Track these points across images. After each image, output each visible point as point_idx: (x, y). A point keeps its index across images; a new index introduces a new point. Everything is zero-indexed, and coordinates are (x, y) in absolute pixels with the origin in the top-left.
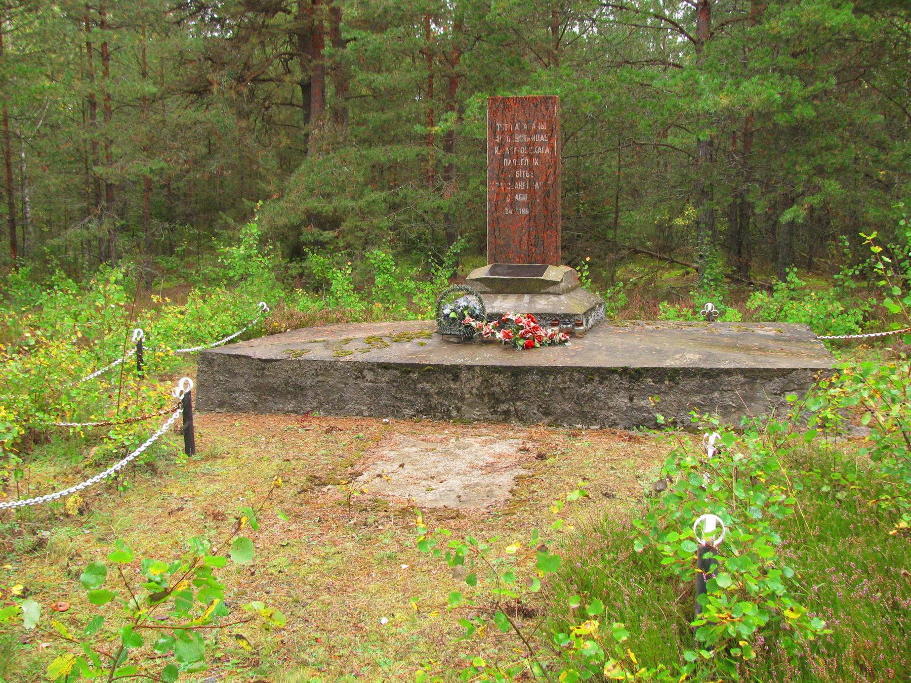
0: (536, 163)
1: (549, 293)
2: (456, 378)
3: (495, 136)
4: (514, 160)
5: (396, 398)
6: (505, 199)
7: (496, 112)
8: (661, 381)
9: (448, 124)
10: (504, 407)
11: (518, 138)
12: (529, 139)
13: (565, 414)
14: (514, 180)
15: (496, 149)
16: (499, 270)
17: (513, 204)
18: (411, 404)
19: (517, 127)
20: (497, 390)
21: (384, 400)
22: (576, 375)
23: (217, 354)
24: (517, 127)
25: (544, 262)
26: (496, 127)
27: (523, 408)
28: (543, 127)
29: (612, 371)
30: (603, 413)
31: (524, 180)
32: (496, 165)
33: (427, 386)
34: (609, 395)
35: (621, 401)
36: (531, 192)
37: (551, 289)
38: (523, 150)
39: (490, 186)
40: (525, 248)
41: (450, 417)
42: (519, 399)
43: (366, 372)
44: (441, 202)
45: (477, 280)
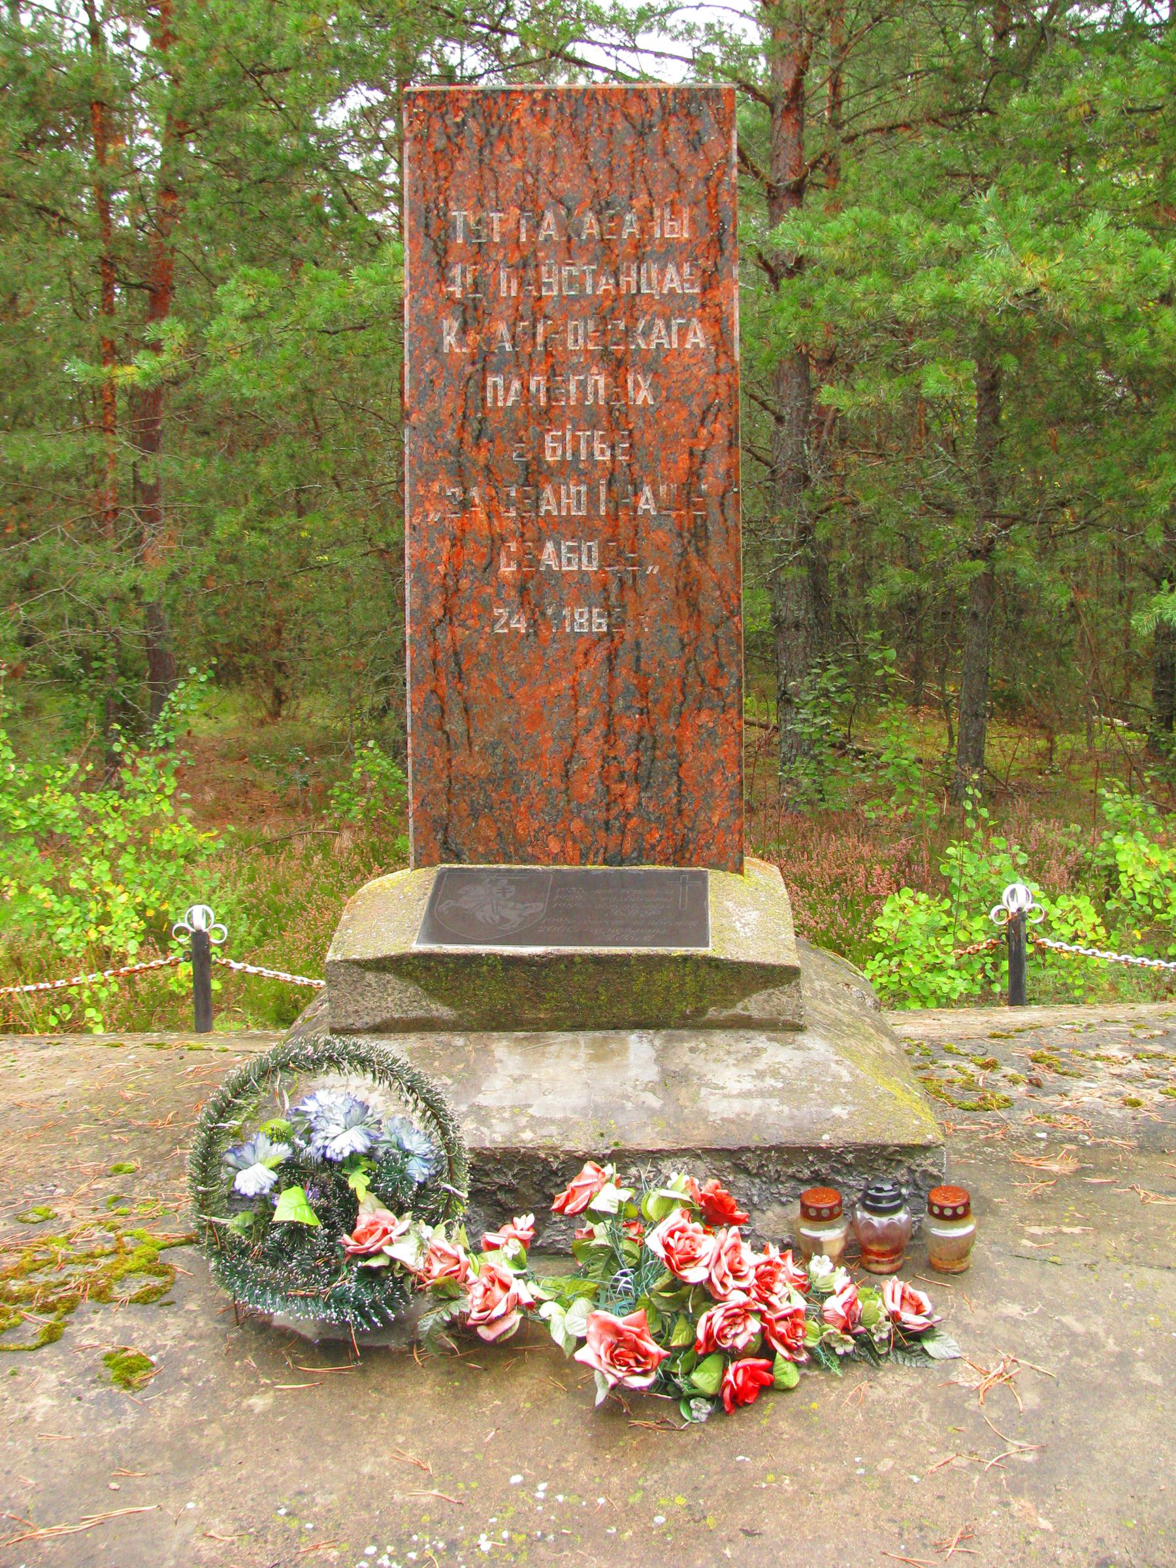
0: (643, 396)
3: (443, 268)
4: (537, 382)
6: (491, 564)
9: (165, 358)
11: (555, 280)
12: (605, 284)
14: (534, 474)
15: (450, 328)
16: (474, 899)
17: (531, 590)
19: (550, 227)
24: (550, 227)
25: (679, 855)
26: (448, 225)
31: (583, 476)
32: (447, 404)
36: (618, 534)
37: (754, 1005)
38: (578, 338)
39: (419, 502)
40: (589, 789)
44: (141, 578)
45: (380, 965)
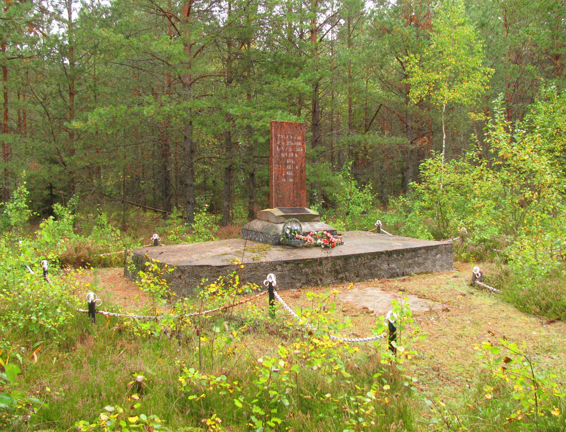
1: (315, 221)
2: (321, 264)
5: (293, 278)
7: (277, 128)
8: (398, 256)
10: (341, 276)
11: (288, 143)
13: (365, 275)
14: (286, 164)
15: (278, 147)
17: (286, 177)
18: (300, 280)
20: (338, 267)
21: (287, 280)
22: (369, 257)
23: (187, 266)
27: (348, 275)
28: (299, 138)
29: (382, 253)
30: (379, 272)
32: (277, 156)
33: (307, 270)
34: (381, 264)
35: (385, 266)
36: (294, 170)
37: (316, 219)
38: (290, 150)
41: (318, 285)
42: (347, 271)
43: (277, 267)
